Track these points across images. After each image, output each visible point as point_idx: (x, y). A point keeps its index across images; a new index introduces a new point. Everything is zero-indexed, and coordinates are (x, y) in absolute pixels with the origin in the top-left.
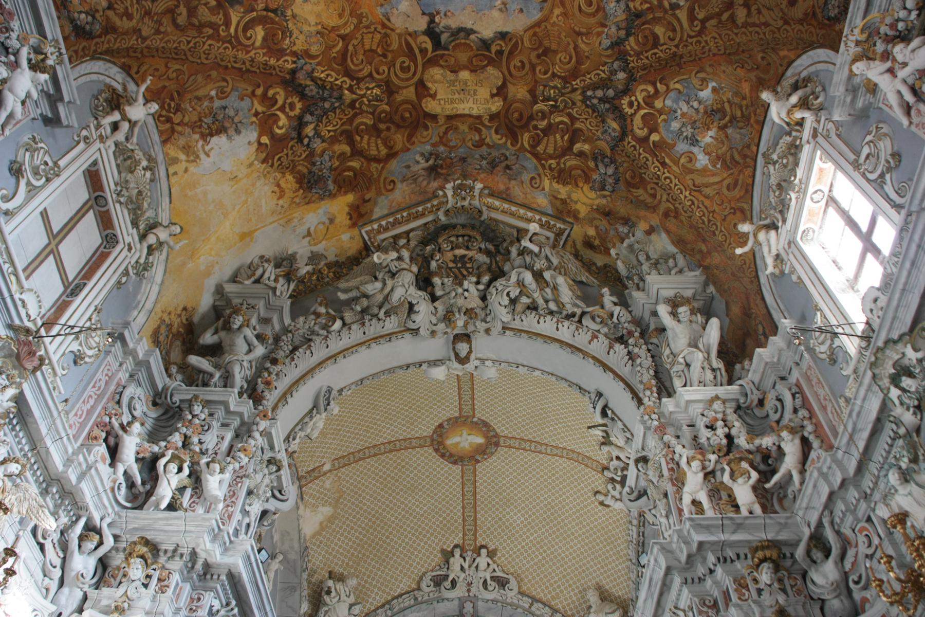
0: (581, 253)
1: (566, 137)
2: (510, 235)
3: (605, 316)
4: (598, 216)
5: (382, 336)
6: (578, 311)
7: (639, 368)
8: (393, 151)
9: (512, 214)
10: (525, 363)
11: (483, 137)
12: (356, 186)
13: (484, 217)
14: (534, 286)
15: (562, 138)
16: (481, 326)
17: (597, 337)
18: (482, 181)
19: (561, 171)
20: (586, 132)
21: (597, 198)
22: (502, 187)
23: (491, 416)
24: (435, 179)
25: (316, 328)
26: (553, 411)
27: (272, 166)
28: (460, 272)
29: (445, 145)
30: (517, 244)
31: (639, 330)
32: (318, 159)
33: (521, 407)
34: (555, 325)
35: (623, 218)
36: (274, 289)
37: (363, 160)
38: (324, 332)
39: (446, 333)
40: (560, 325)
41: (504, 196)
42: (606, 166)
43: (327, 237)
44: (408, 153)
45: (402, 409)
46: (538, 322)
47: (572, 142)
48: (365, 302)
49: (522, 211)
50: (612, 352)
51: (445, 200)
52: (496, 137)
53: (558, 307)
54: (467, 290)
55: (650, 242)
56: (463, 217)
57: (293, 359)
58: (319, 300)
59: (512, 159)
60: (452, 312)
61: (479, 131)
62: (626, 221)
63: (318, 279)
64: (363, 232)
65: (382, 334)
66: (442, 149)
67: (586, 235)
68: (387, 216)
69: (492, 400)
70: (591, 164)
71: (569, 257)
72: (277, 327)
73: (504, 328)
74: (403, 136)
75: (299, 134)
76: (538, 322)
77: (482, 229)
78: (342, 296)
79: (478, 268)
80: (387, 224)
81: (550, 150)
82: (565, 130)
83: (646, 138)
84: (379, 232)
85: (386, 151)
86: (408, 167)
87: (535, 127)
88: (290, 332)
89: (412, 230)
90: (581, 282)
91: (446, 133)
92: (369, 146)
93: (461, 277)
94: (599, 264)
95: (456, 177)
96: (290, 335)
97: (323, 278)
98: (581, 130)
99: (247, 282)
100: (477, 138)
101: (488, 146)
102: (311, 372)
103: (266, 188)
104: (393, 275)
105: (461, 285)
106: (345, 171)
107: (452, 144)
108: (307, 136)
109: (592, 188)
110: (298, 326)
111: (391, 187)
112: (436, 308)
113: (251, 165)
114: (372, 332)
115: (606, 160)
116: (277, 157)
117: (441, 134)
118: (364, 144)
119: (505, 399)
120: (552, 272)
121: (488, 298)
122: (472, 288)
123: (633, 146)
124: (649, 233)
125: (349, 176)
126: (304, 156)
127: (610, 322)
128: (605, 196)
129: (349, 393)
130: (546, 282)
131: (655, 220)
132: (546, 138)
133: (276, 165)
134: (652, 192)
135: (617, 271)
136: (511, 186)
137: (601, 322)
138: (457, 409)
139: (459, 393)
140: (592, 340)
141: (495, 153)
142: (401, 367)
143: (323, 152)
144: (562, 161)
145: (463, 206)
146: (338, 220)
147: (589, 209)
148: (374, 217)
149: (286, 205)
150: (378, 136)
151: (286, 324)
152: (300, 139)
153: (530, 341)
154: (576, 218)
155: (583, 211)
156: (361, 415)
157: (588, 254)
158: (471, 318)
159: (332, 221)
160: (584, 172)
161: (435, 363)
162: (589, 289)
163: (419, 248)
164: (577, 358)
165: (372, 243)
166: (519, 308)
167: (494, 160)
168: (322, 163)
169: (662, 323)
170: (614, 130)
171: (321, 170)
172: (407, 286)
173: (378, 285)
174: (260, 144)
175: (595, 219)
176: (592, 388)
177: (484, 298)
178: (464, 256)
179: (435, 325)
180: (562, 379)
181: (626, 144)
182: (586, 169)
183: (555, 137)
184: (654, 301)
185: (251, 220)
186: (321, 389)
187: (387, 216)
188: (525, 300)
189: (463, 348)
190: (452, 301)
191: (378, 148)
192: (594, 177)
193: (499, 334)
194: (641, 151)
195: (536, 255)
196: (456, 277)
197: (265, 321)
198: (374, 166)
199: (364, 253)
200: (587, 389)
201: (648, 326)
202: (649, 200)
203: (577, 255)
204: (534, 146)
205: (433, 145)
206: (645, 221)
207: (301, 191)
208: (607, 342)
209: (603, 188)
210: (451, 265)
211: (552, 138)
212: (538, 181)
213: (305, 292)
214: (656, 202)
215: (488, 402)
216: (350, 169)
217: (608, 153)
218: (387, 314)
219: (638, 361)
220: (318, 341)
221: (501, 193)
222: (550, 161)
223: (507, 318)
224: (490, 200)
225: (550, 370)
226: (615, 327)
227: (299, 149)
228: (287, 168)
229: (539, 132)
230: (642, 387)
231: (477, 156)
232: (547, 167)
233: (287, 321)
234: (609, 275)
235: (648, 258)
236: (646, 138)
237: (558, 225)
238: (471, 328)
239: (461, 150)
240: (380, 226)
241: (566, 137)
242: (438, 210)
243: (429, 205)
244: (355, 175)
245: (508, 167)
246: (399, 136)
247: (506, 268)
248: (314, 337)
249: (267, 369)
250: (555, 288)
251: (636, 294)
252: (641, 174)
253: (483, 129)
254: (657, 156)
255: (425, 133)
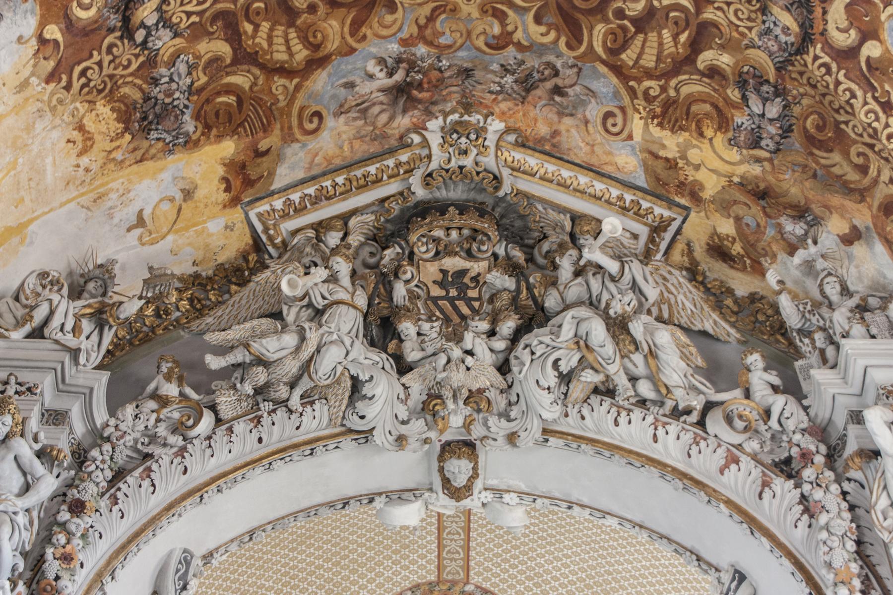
0: (703, 267)
1: (683, 38)
2: (556, 226)
3: (754, 416)
4: (743, 198)
5: (296, 446)
6: (697, 403)
7: (824, 535)
8: (321, 54)
9: (563, 185)
10: (586, 501)
11: (510, 28)
12: (241, 125)
13: (506, 189)
14: (609, 349)
15: (675, 37)
16: (499, 427)
17: (737, 461)
18: (502, 116)
19: (668, 104)
20: (725, 30)
21: (741, 162)
22: (543, 130)
23: (503, 581)
24: (405, 111)
25: (162, 430)
26: (635, 577)
27: (68, 88)
28: (456, 308)
29: (430, 44)
30: (574, 252)
31: (823, 449)
32: (163, 71)
33: (566, 566)
34: (651, 431)
35: (794, 207)
36: (75, 353)
37: (257, 72)
38: (176, 440)
39: (426, 441)
40: (661, 432)
41: (547, 147)
42: (765, 101)
43: (176, 227)
44: (350, 59)
45: (319, 567)
46: (616, 423)
47: (696, 47)
48: (260, 376)
49: (583, 180)
50: (767, 494)
51: (425, 152)
52: (535, 30)
53: (658, 391)
54: (470, 353)
55: (850, 257)
56: (460, 187)
57: (115, 501)
58: (164, 369)
59: (569, 74)
60: (439, 397)
61: (501, 16)
62: (800, 212)
63: (157, 315)
64: (252, 215)
65: (296, 440)
66: (421, 50)
67: (715, 233)
68: (303, 182)
69: (507, 551)
70: (734, 94)
71: (679, 277)
72: (79, 428)
73: (545, 431)
74: (343, 23)
75: (126, 20)
76: (616, 423)
77: (497, 212)
78: (214, 362)
79: (491, 300)
80: (302, 199)
81: (649, 61)
82: (682, 24)
83: (852, 52)
84: (285, 216)
85: (305, 53)
86: (351, 85)
87: (620, 14)
88: (108, 439)
89: (354, 212)
90: (704, 333)
91: (431, 19)
92: (270, 44)
93: (456, 319)
94: (741, 291)
95: (448, 107)
96: (107, 447)
97: (167, 313)
98: (715, 25)
99: (17, 335)
100: (497, 30)
101: (519, 46)
102: (151, 524)
103: (55, 134)
104: (318, 313)
105: (458, 339)
106: (219, 94)
107: (443, 41)
108: (143, 25)
109: (732, 142)
110: (123, 427)
111: (313, 126)
112: (406, 388)
113: (24, 85)
114: (275, 437)
115: (765, 88)
116: (78, 69)
117: (422, 21)
118: (261, 40)
119: (532, 550)
120: (645, 318)
121: (515, 369)
122: (481, 347)
123: (824, 65)
124: (851, 238)
125: (228, 104)
126: (134, 66)
127: (762, 428)
128: (758, 160)
129: (224, 557)
130: (634, 342)
131: (863, 217)
132: (641, 37)
133: (76, 85)
134: (860, 161)
135: (777, 312)
136: (562, 128)
137: (746, 429)
138: (433, 567)
139: (439, 538)
140: (727, 466)
141: (533, 62)
142: (331, 505)
143: (176, 56)
144: (673, 83)
145: (461, 168)
146: (200, 194)
147: (723, 181)
148: (276, 185)
149: (94, 167)
150: (291, 24)
151: (99, 423)
152: (127, 30)
153: (599, 460)
154: (695, 197)
155: (711, 186)
156: (234, 581)
157: (716, 270)
158: (479, 411)
159: (188, 194)
160: (716, 107)
161: (400, 496)
162: (719, 346)
163: (367, 249)
164: (696, 501)
165: (271, 239)
166: (577, 390)
167: (530, 75)
168: (172, 80)
169: (872, 441)
170: (786, 30)
171: (169, 94)
172: (348, 342)
173: (290, 340)
174: (42, 41)
175: (735, 202)
176: (724, 562)
177: (504, 368)
178: (462, 273)
179: (403, 423)
180: (662, 537)
181: (809, 59)
182: (721, 104)
183: (660, 36)
184: (856, 390)
185: (22, 200)
186: (170, 555)
187: (303, 182)
188: (589, 377)
189: (460, 469)
190: (441, 376)
191: (289, 48)
192: (738, 120)
193: (536, 443)
194: (841, 77)
195: (613, 279)
196: (447, 320)
197: (55, 417)
198: (279, 82)
199: (253, 257)
200: (714, 561)
201: (843, 438)
202: (853, 176)
203: (693, 273)
204: (615, 52)
205: (404, 42)
206: (842, 216)
207: (128, 137)
208: (757, 472)
209: (756, 143)
210: (436, 291)
211: (653, 36)
212: (619, 120)
213: (131, 343)
214: (866, 181)
215: (497, 555)
216: (229, 90)
217: (772, 75)
218: (308, 399)
219: (823, 519)
220: (166, 460)
221: (541, 140)
222: (647, 83)
223: (551, 413)
224: (518, 155)
225: (637, 519)
226: (773, 437)
227: (125, 51)
228: (100, 92)
229: (626, 22)
230: (831, 577)
231: (495, 67)
232: (640, 94)
233: (101, 415)
234: (761, 317)
235: (845, 291)
236: (852, 52)
237: (658, 211)
238: (477, 431)
239: (461, 54)
240: (289, 203)
241: (683, 38)
242: (409, 172)
243: (391, 162)
244: (240, 101)
245: (558, 91)
246: (334, 23)
247: (551, 301)
248: (157, 451)
249: (63, 525)
250: (652, 354)
251: (821, 375)
252: (837, 123)
253: (510, 12)
254: (874, 89)
255: (389, 18)
